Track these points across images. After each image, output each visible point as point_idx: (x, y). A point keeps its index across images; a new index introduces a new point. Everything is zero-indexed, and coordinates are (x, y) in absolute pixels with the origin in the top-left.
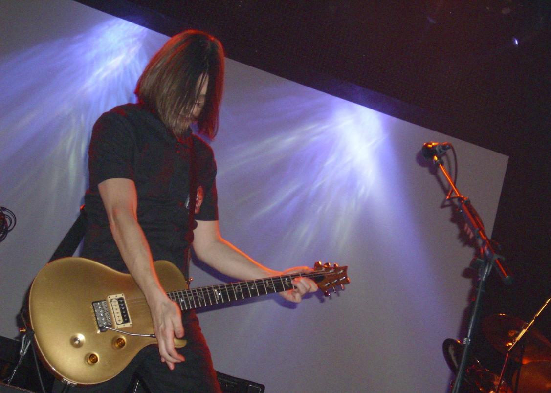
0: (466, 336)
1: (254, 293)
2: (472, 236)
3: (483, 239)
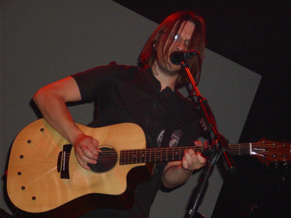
0: (192, 208)
1: (127, 161)
2: (205, 129)
3: (215, 134)
